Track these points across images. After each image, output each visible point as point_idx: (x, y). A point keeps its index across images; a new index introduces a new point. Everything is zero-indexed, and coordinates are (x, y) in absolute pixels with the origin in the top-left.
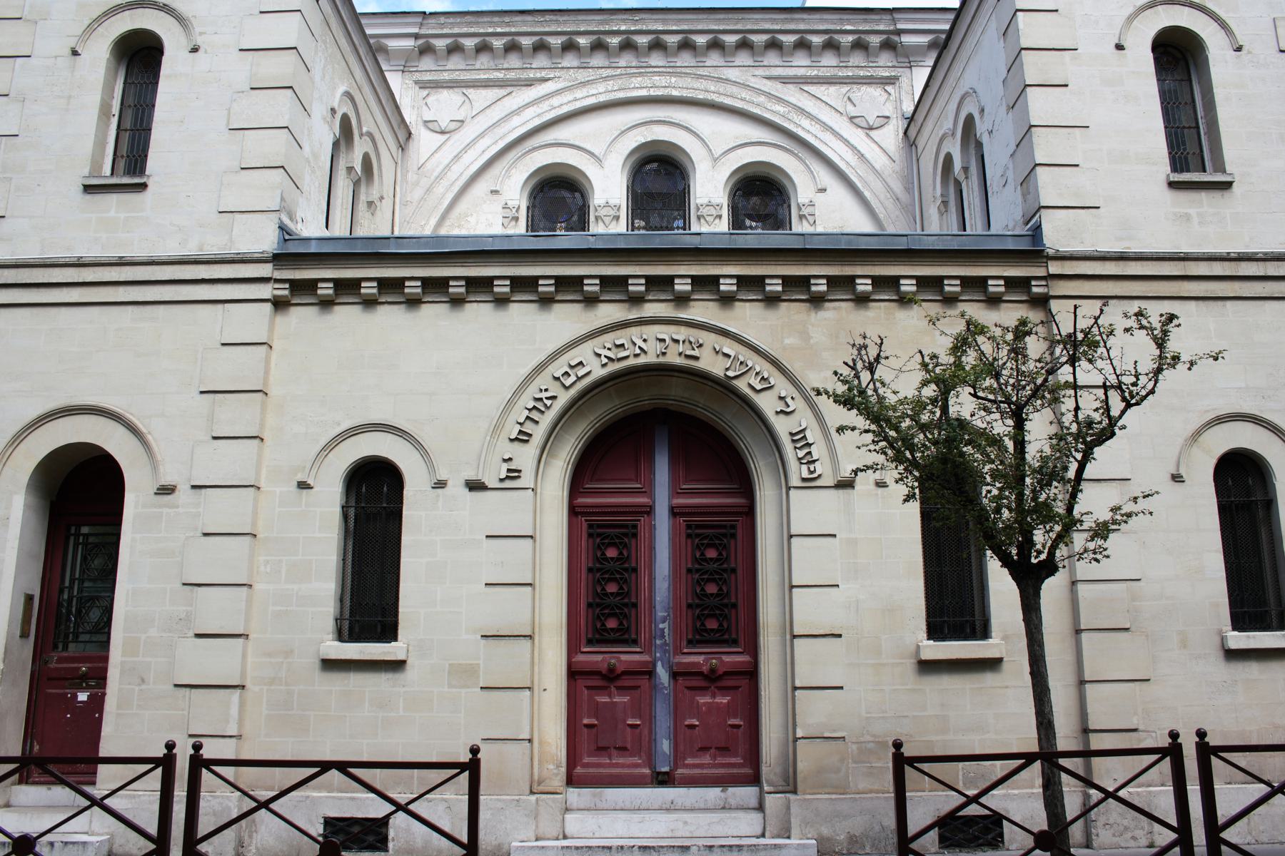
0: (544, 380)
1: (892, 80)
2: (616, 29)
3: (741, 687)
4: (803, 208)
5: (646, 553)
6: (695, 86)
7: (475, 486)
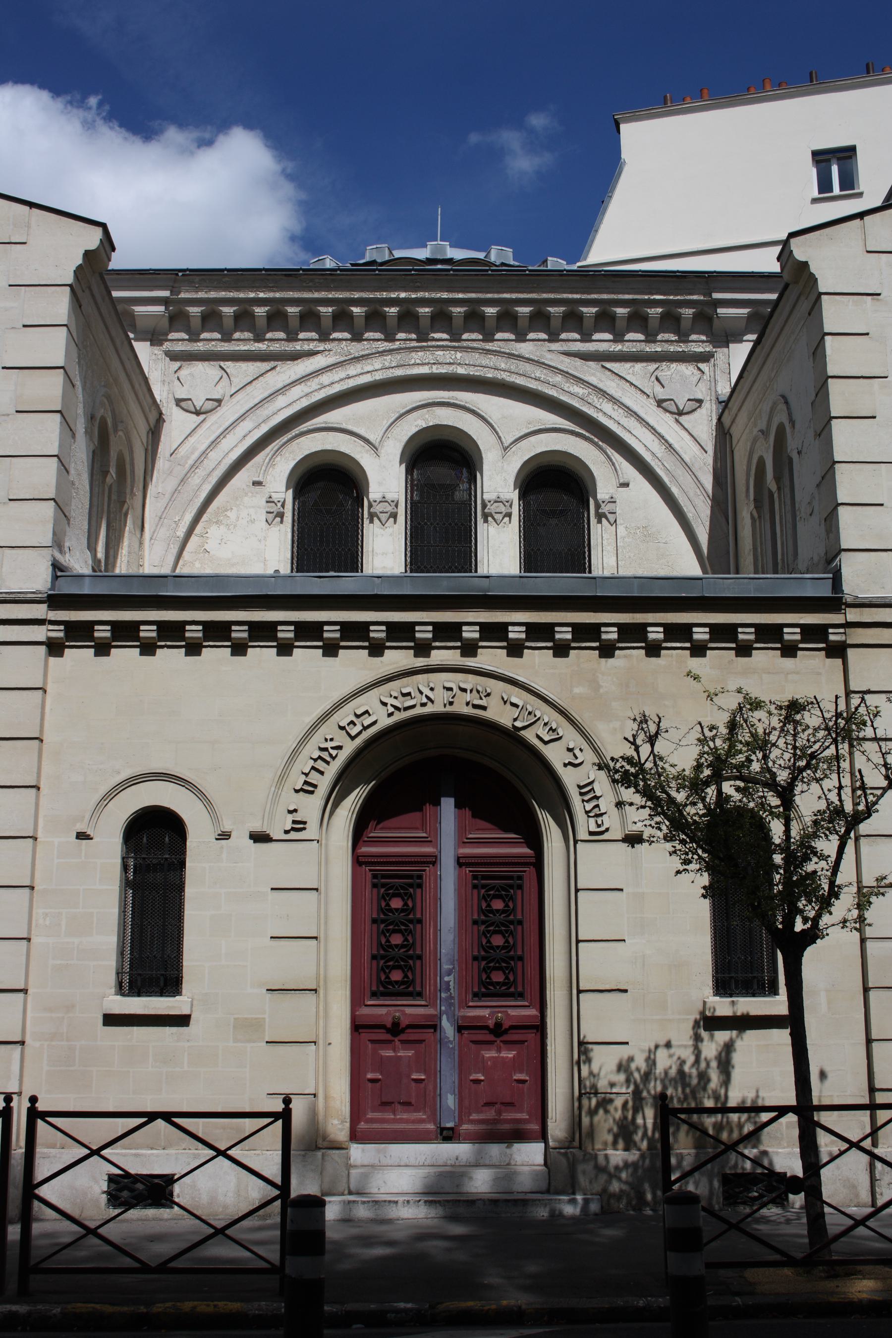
0: (329, 729)
1: (705, 358)
2: (395, 296)
3: (526, 1041)
4: (603, 505)
5: (432, 904)
6: (484, 363)
7: (259, 838)
